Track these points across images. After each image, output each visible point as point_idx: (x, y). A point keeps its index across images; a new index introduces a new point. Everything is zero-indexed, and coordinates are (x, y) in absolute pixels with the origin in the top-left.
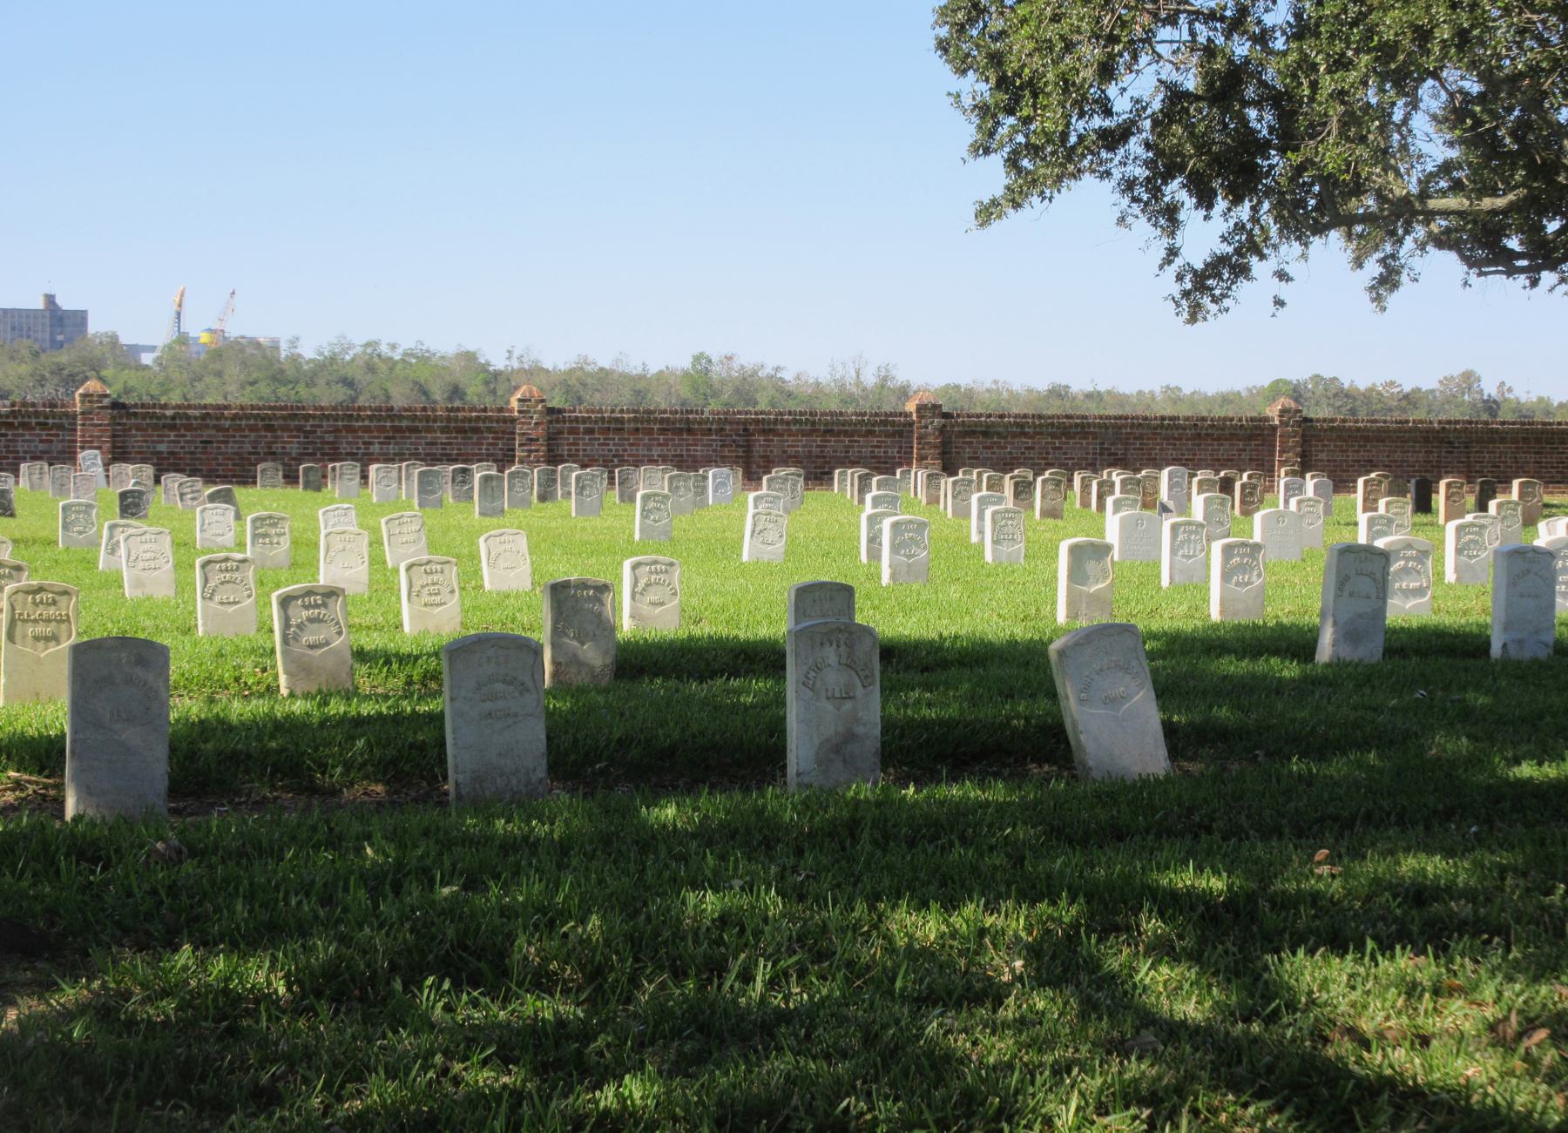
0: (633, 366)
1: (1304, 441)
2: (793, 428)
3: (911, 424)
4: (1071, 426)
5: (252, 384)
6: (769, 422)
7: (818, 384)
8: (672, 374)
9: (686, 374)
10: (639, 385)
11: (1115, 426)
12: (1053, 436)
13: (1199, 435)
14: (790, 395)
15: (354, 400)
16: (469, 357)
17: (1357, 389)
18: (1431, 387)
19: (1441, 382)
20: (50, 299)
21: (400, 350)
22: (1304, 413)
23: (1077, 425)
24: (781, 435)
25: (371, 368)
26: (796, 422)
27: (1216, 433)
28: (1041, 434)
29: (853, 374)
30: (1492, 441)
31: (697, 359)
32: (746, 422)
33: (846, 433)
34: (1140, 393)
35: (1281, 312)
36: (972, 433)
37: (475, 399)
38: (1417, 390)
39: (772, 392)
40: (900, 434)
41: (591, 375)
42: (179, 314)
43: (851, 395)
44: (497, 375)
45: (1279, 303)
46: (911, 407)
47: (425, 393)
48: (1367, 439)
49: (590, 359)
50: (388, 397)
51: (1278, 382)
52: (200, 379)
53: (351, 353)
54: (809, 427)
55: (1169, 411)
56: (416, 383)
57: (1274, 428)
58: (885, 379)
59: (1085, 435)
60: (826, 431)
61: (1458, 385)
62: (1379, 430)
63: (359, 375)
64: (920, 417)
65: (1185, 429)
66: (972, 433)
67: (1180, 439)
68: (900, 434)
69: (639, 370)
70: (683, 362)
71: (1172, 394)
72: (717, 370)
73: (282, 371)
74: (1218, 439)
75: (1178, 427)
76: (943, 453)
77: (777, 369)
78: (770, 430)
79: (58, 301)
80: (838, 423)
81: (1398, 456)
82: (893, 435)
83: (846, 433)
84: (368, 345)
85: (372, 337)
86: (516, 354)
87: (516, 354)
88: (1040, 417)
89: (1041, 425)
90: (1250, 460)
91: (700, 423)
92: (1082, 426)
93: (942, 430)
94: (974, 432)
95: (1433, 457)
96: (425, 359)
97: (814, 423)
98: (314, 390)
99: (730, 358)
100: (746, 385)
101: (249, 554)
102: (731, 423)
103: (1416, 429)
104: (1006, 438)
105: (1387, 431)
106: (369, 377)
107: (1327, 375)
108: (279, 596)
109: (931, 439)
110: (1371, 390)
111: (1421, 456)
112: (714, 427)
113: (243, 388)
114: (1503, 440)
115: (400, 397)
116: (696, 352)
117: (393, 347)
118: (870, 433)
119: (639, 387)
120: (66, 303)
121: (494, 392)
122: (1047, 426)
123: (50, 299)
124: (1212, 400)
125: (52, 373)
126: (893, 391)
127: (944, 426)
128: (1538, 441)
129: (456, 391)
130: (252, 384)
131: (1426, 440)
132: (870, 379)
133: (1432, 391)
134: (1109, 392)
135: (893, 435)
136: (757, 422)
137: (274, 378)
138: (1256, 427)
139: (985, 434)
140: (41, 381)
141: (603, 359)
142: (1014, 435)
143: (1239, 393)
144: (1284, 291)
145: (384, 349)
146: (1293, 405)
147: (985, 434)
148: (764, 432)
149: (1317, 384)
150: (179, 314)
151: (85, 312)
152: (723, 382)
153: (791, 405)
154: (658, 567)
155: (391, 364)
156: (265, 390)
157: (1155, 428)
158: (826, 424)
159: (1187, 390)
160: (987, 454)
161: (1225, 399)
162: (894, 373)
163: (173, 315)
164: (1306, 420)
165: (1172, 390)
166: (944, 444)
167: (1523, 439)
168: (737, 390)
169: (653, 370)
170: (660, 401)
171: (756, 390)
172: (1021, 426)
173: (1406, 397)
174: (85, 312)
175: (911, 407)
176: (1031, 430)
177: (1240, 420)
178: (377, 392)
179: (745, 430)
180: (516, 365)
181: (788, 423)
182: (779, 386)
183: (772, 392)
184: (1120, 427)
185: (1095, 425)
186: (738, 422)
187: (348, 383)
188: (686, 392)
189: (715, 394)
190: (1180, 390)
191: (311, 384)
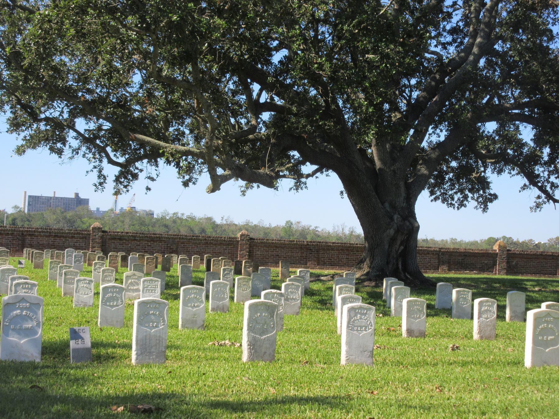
0: (266, 223)
1: (250, 247)
2: (42, 234)
3: (90, 235)
4: (154, 238)
5: (133, 225)
6: (32, 231)
7: (329, 233)
8: (279, 228)
9: (284, 228)
10: (267, 231)
11: (172, 238)
12: (148, 241)
13: (207, 243)
14: (319, 236)
15: (168, 232)
16: (209, 219)
17: (518, 242)
18: (545, 242)
19: (549, 240)
20: (77, 195)
21: (185, 216)
22: (251, 236)
23: (157, 237)
24: (37, 237)
25: (174, 222)
26: (43, 232)
27: (214, 242)
28: (143, 240)
29: (341, 230)
30: (328, 250)
31: (287, 222)
32: (22, 231)
33: (63, 237)
34: (442, 240)
35: (149, 192)
36: (115, 239)
37: (209, 234)
38: (539, 243)
39: (312, 235)
40: (85, 238)
41: (251, 227)
42: (116, 201)
43: (340, 237)
44: (217, 225)
45: (148, 189)
46: (496, 248)
47: (192, 231)
48: (276, 247)
49: (251, 221)
50: (180, 232)
51: (490, 238)
52: (115, 223)
53: (169, 216)
54: (48, 234)
55: (452, 247)
56: (189, 227)
57: (238, 242)
58: (352, 232)
59: (161, 241)
60: (55, 236)
61: (555, 242)
62: (281, 244)
63: (170, 224)
64: (93, 232)
65: (201, 240)
66: (115, 239)
67: (200, 244)
68: (85, 238)
69: (268, 226)
70: (282, 223)
71: (454, 241)
72: (294, 227)
73: (144, 222)
74: (215, 245)
75: (199, 240)
76: (102, 246)
77: (316, 227)
78: (32, 235)
79: (80, 195)
80: (60, 233)
81: (289, 254)
82: (82, 238)
83: (63, 237)
84: (174, 214)
85: (176, 211)
86: (225, 218)
87: (225, 218)
88: (143, 234)
89: (142, 237)
90: (229, 253)
91: (4, 231)
92: (159, 238)
93: (102, 237)
94: (115, 238)
95: (304, 255)
96: (193, 219)
97: (50, 233)
98: (155, 229)
99: (298, 223)
100: (304, 232)
101: (124, 286)
102: (17, 231)
103: (297, 244)
104: (128, 241)
105: (284, 244)
106: (173, 225)
107: (508, 236)
108: (138, 302)
109: (97, 240)
110: (523, 242)
111: (299, 254)
112: (10, 232)
113: (130, 226)
114: (333, 249)
115: (184, 231)
116: (288, 220)
117: (183, 214)
118: (73, 237)
119: (266, 231)
120: (82, 196)
121: (216, 231)
122: (145, 237)
123: (77, 195)
124: (467, 244)
125: (63, 219)
126: (355, 236)
127: (103, 236)
128: (347, 250)
129: (203, 231)
130: (133, 225)
131: (301, 248)
132: (347, 232)
133: (545, 243)
134: (431, 239)
135: (82, 238)
136: (27, 231)
137: (141, 224)
138: (231, 241)
139: (120, 239)
140: (59, 222)
141: (255, 221)
142: (132, 240)
143: (477, 242)
144: (150, 184)
145: (180, 215)
146: (246, 233)
147: (120, 239)
148: (30, 235)
149: (504, 239)
150: (116, 201)
151: (88, 199)
152: (296, 231)
153: (319, 240)
154: (27, 286)
155: (181, 219)
156: (137, 227)
157: (190, 239)
158: (55, 233)
159: (459, 240)
160: (120, 247)
161: (472, 244)
162: (355, 230)
163: (114, 201)
164: (251, 239)
165: (454, 240)
166: (102, 242)
167: (341, 249)
168: (300, 234)
169: (273, 225)
170: (273, 236)
171: (307, 234)
172: (135, 237)
173: (536, 245)
174: (88, 199)
175: (496, 248)
176: (138, 239)
177: (225, 238)
178: (176, 230)
179: (22, 234)
180: (225, 222)
181: (40, 232)
182: (315, 232)
183: (312, 235)
184: (175, 239)
185: (164, 238)
186: (20, 231)
187: (166, 226)
188: (282, 234)
189: (293, 235)
190: (456, 239)
191: (153, 226)
